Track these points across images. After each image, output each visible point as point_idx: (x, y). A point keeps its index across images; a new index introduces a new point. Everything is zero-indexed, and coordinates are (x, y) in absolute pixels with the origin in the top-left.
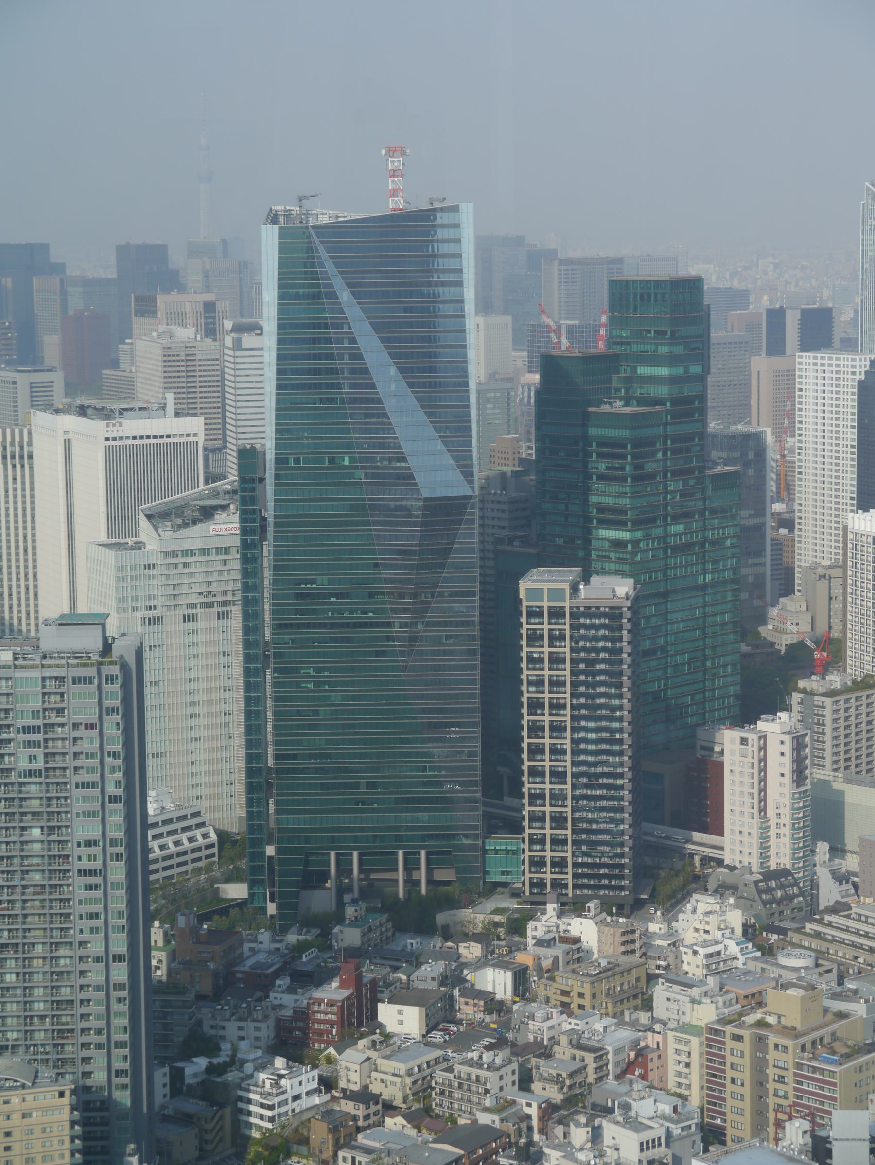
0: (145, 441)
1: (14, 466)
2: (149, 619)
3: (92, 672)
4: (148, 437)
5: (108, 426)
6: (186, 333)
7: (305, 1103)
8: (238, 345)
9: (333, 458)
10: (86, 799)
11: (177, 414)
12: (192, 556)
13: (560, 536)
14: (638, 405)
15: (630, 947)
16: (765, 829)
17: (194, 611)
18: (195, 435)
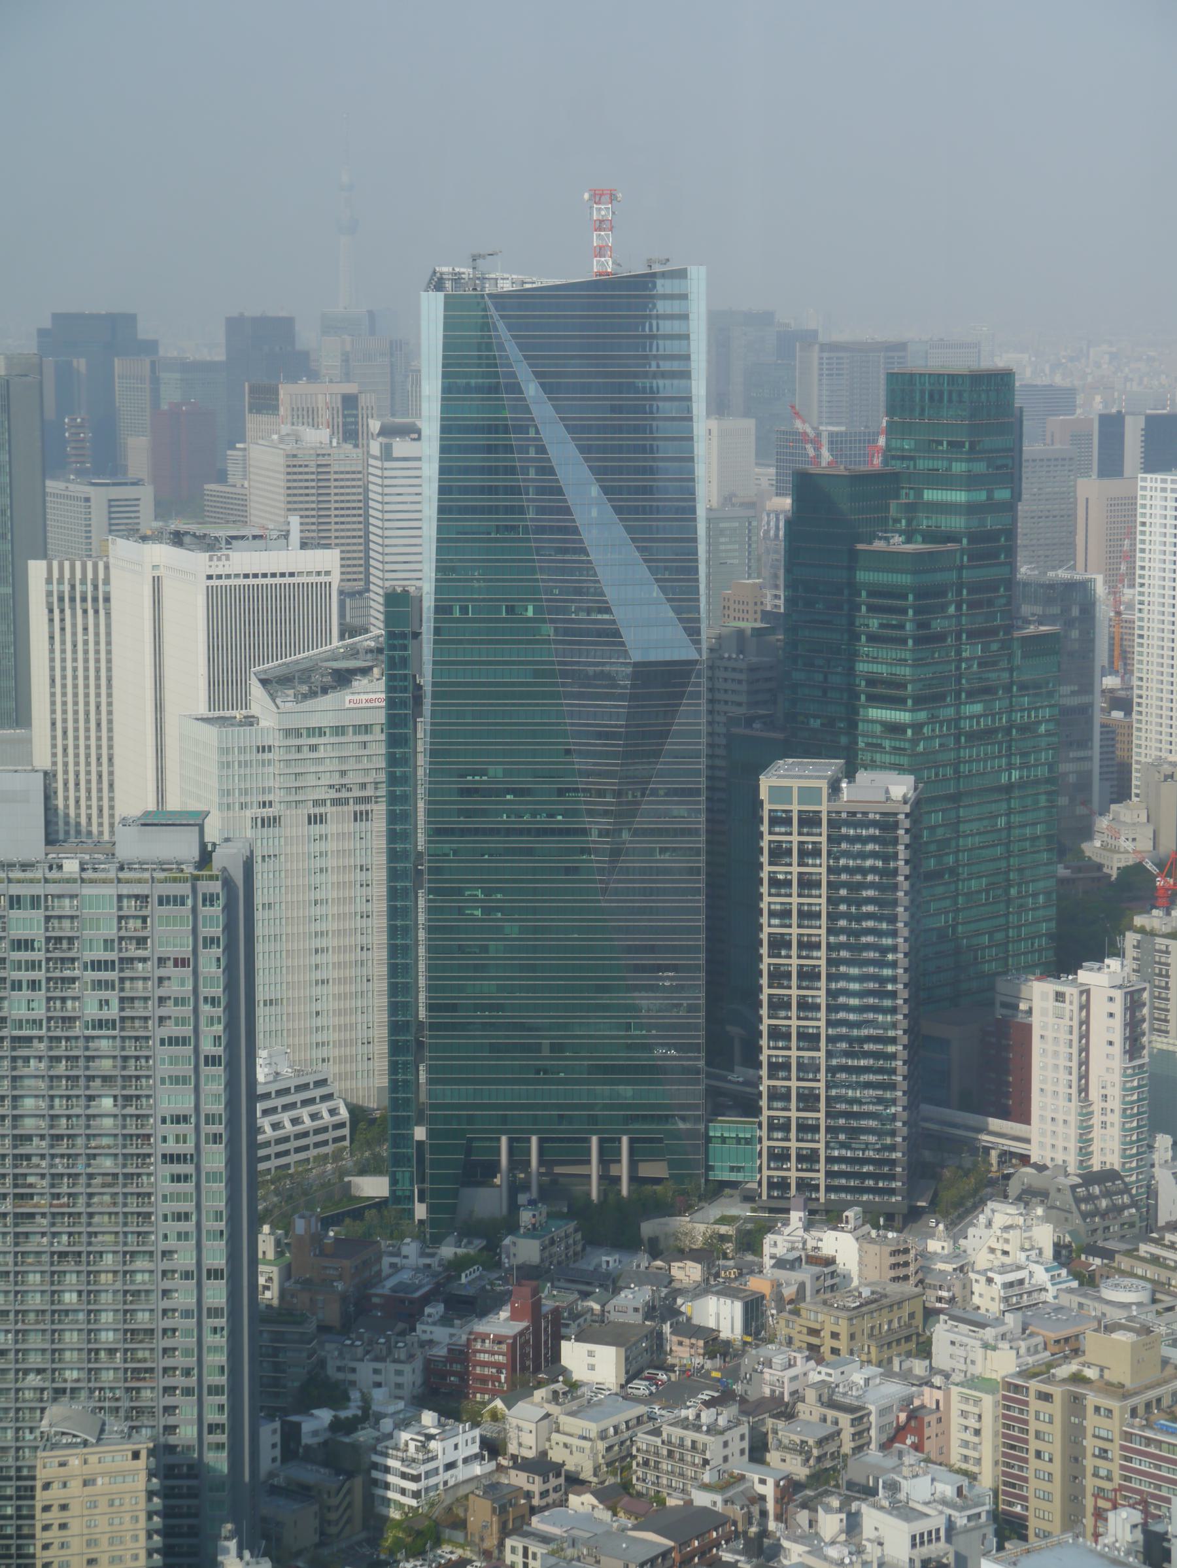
0: (260, 581)
1: (85, 611)
2: (263, 820)
3: (184, 889)
4: (265, 575)
5: (211, 559)
6: (317, 437)
7: (462, 1473)
8: (387, 454)
9: (513, 606)
10: (174, 1060)
11: (304, 545)
12: (320, 736)
13: (815, 717)
14: (924, 542)
15: (901, 1272)
16: (1086, 1115)
17: (322, 810)
18: (328, 573)
